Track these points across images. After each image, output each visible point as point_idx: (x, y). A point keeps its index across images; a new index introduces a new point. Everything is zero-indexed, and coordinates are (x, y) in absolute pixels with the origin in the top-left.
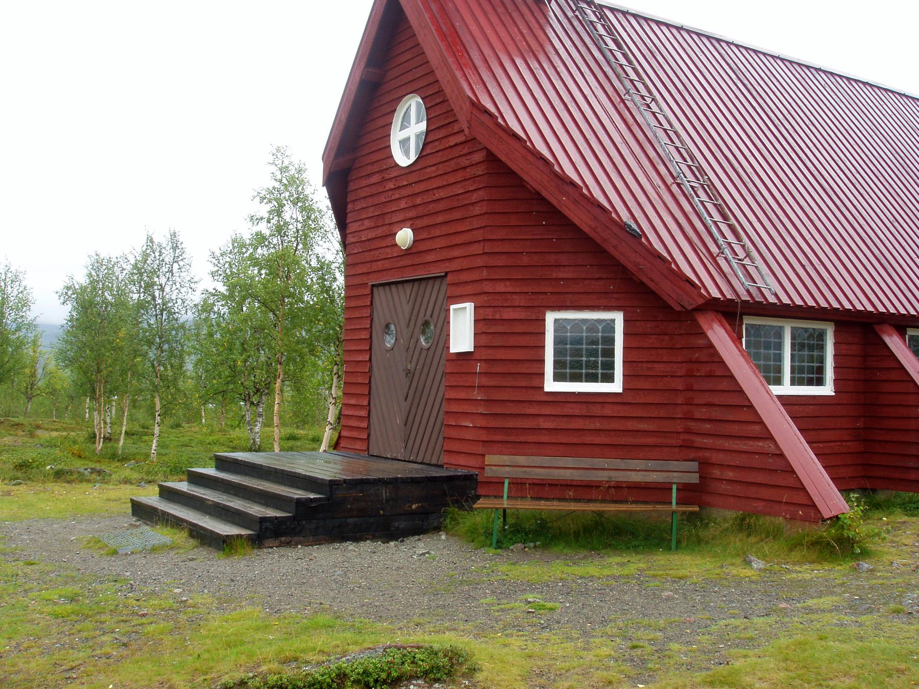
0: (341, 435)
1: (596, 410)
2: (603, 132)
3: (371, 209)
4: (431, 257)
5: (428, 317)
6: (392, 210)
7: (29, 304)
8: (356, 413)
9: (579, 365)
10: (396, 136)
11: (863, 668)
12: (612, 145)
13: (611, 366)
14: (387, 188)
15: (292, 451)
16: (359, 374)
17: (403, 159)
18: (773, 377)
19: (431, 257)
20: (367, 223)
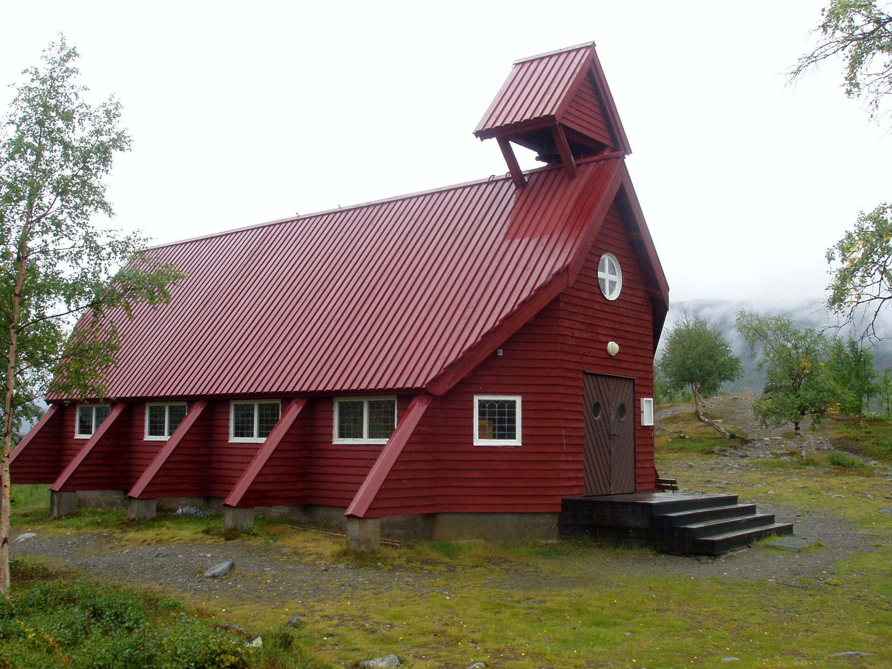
0: (637, 466)
1: (492, 457)
2: (403, 279)
3: (581, 316)
4: (624, 365)
5: (596, 400)
6: (599, 324)
7: (847, 82)
8: (574, 467)
9: (503, 429)
10: (618, 279)
11: (212, 629)
12: (413, 295)
13: (513, 429)
14: (594, 307)
15: (735, 450)
16: (575, 437)
17: (613, 295)
18: (498, 431)
19: (624, 365)
20: (578, 325)
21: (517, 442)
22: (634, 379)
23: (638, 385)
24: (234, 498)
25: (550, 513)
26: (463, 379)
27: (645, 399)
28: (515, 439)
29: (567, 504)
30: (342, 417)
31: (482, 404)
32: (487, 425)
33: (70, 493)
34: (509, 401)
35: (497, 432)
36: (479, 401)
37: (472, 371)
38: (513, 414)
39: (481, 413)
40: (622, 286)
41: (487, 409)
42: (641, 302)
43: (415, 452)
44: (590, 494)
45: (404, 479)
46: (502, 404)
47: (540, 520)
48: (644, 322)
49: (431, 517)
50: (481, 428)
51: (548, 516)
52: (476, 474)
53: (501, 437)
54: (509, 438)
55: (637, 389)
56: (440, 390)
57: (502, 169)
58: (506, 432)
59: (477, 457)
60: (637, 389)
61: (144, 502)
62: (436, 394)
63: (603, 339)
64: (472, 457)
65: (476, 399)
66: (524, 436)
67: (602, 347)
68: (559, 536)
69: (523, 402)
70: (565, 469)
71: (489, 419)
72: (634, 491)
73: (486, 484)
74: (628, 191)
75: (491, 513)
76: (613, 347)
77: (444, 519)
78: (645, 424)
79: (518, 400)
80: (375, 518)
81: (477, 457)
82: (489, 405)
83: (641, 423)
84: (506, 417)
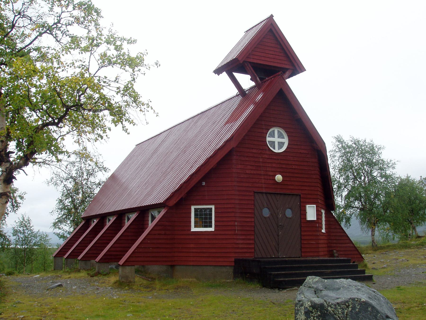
21: (212, 229)
22: (300, 195)
23: (302, 198)
24: (80, 258)
25: (229, 266)
26: (182, 198)
27: (308, 205)
28: (212, 227)
29: (237, 261)
30: (196, 224)
31: (196, 210)
32: (199, 220)
33: (72, 259)
34: (200, 208)
35: (203, 224)
36: (195, 209)
37: (187, 193)
38: (211, 215)
39: (196, 215)
40: (288, 144)
41: (199, 213)
42: (307, 152)
43: (158, 234)
44: (260, 256)
45: (151, 248)
46: (205, 209)
47: (224, 269)
48: (253, 160)
49: (172, 266)
50: (196, 222)
51: (228, 267)
52: (192, 246)
53: (206, 226)
54: (209, 227)
55: (302, 200)
56: (172, 203)
57: (235, 91)
58: (208, 224)
59: (193, 237)
60: (302, 200)
61: (84, 262)
62: (169, 206)
63: (271, 174)
64: (191, 237)
65: (193, 208)
66: (216, 226)
67: (271, 178)
68: (233, 278)
69: (215, 208)
70: (237, 243)
71: (200, 218)
72: (300, 256)
73: (197, 251)
74: (286, 92)
75: (200, 265)
76: (279, 178)
77: (178, 268)
78: (308, 220)
79: (213, 207)
80: (130, 266)
81: (193, 237)
82: (200, 211)
83: (306, 218)
84: (208, 216)
